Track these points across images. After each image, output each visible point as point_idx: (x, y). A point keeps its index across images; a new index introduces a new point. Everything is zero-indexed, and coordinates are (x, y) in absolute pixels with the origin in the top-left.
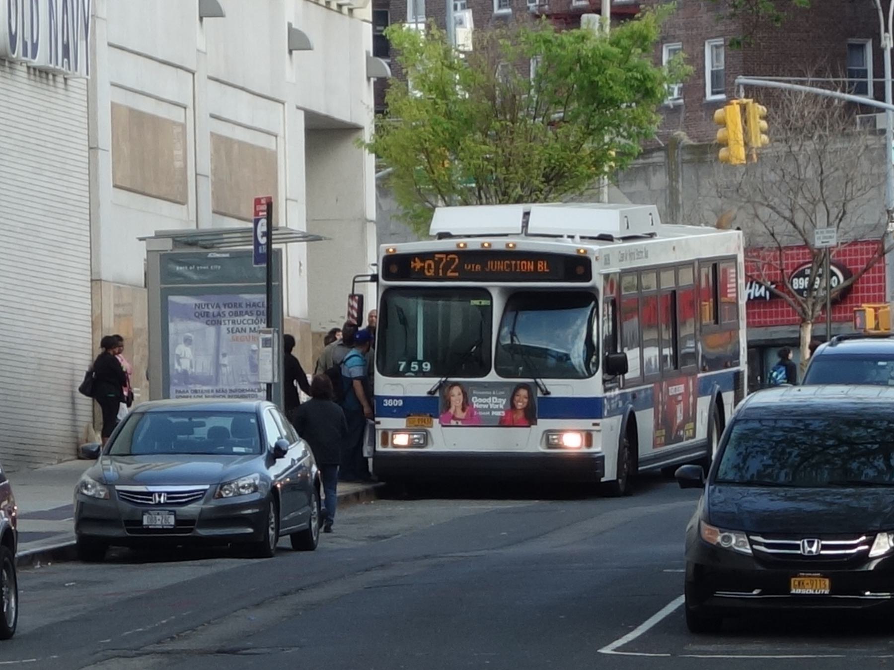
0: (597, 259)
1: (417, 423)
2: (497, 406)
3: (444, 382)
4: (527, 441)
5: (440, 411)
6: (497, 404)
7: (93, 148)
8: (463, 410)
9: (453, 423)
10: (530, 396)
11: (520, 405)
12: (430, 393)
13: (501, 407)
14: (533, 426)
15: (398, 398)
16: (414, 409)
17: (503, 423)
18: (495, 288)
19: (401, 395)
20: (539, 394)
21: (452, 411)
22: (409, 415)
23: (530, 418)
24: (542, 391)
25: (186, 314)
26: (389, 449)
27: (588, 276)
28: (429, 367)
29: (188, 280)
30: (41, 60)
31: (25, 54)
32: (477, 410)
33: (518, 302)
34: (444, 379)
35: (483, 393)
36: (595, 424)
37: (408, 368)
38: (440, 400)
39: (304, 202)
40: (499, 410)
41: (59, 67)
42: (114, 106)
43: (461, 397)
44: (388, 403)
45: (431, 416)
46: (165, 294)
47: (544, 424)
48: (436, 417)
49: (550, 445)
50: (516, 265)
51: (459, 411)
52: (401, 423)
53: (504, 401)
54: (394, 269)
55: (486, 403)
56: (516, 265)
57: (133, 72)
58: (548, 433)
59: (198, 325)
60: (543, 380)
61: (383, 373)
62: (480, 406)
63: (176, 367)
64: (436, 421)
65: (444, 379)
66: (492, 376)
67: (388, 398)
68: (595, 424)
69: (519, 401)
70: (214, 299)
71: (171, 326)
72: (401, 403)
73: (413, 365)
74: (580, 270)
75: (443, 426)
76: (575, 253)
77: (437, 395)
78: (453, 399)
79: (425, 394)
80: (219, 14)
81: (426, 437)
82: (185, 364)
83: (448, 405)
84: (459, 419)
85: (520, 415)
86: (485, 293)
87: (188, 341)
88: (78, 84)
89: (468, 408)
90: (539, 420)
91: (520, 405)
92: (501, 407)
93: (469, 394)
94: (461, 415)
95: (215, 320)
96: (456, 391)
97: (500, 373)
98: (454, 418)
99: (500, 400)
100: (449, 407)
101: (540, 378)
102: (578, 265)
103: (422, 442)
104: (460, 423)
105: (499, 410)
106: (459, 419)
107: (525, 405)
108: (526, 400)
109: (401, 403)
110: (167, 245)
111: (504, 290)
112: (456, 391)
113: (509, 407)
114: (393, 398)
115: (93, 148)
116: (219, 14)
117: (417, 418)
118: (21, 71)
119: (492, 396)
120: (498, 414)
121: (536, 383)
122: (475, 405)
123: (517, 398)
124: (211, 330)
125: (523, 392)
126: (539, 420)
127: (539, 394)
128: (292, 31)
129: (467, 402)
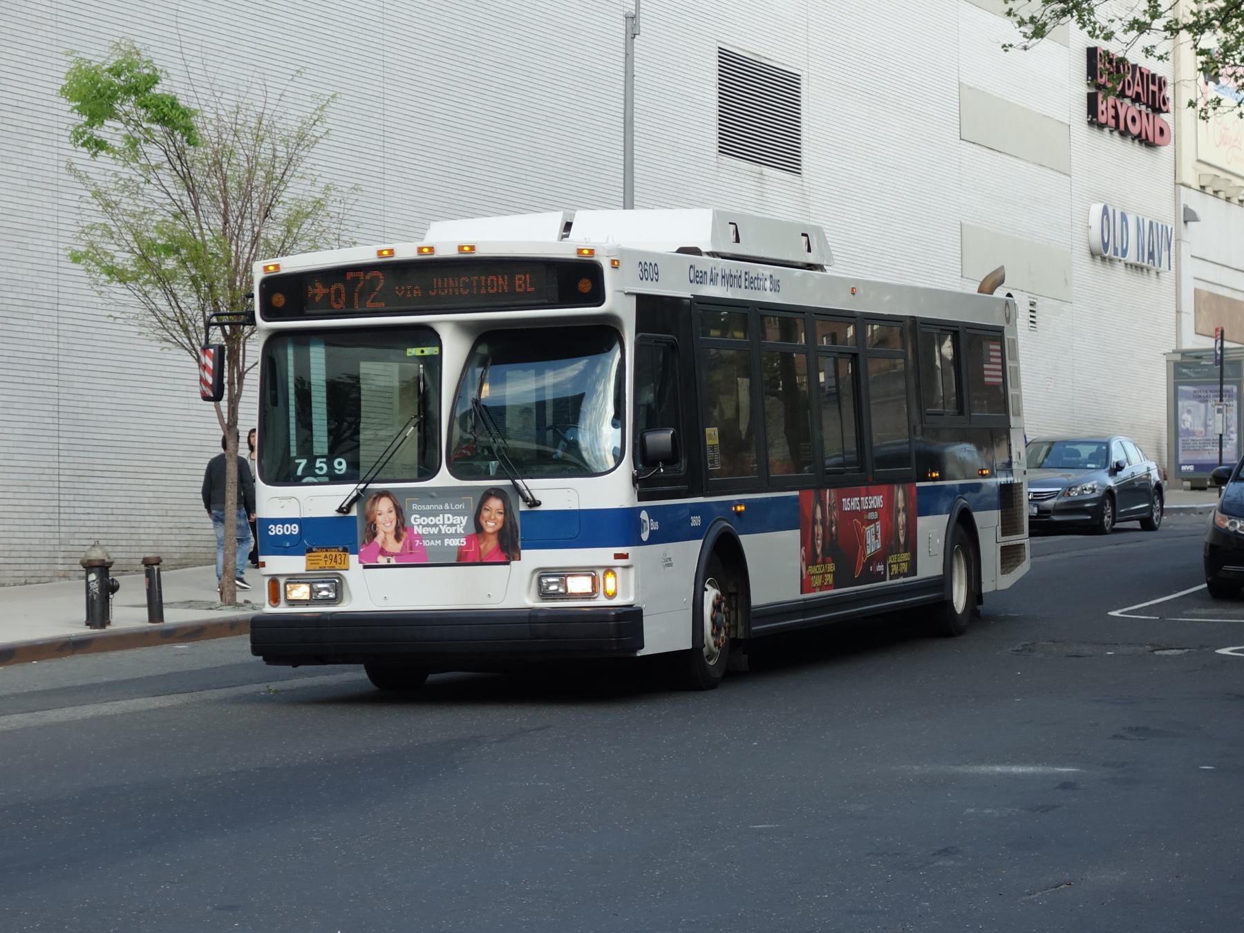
0: (615, 265)
1: (322, 564)
2: (452, 530)
3: (363, 490)
4: (507, 588)
5: (359, 541)
6: (451, 527)
7: (1178, 312)
8: (398, 538)
9: (382, 560)
10: (507, 511)
11: (491, 526)
12: (340, 510)
13: (460, 530)
14: (513, 563)
15: (291, 521)
16: (315, 536)
17: (464, 559)
18: (445, 324)
19: (297, 516)
20: (523, 507)
21: (379, 540)
22: (310, 551)
23: (508, 548)
24: (526, 500)
25: (1188, 396)
26: (283, 609)
27: (597, 296)
28: (344, 466)
29: (1190, 377)
30: (1131, 257)
31: (1116, 254)
32: (421, 537)
33: (498, 348)
34: (362, 486)
35: (429, 507)
36: (617, 556)
37: (310, 470)
38: (358, 521)
39: (965, 291)
40: (455, 535)
41: (1145, 264)
42: (1196, 291)
43: (393, 515)
44: (276, 530)
45: (345, 550)
46: (1176, 385)
47: (533, 559)
48: (355, 552)
49: (544, 595)
50: (479, 282)
51: (391, 538)
52: (296, 564)
53: (464, 520)
54: (279, 300)
55: (436, 525)
56: (479, 282)
57: (1211, 273)
58: (543, 573)
59: (1195, 403)
60: (527, 481)
61: (268, 481)
62: (425, 531)
63: (1182, 426)
64: (353, 559)
65: (362, 486)
66: (444, 478)
67: (276, 521)
68: (617, 556)
69: (490, 519)
70: (1204, 388)
71: (1180, 403)
72: (295, 529)
73: (318, 465)
74: (585, 286)
75: (365, 567)
76: (575, 257)
77: (354, 512)
78: (379, 518)
79: (332, 513)
80: (1196, 219)
81: (339, 588)
82: (1188, 425)
83: (372, 531)
84: (392, 555)
85: (490, 544)
86: (428, 335)
87: (1189, 412)
88: (1168, 277)
89: (405, 534)
90: (524, 553)
91: (491, 526)
92: (460, 530)
93: (406, 510)
94: (394, 546)
95: (1204, 400)
96: (385, 505)
97: (455, 472)
98: (383, 552)
99: (458, 519)
100: (375, 535)
101: (522, 478)
102: (579, 278)
103: (332, 595)
104: (393, 562)
105: (455, 535)
106: (392, 555)
107: (499, 525)
108: (500, 517)
109: (295, 529)
110: (1178, 357)
111: (464, 327)
112: (385, 505)
113: (472, 530)
114: (283, 521)
115: (1178, 312)
116: (1196, 219)
117: (323, 554)
118: (1121, 266)
119: (444, 512)
120: (455, 542)
121: (516, 486)
122: (417, 530)
123: (486, 514)
124: (1202, 406)
125: (495, 504)
126: (524, 553)
127: (523, 507)
128: (1186, 209)
129: (403, 524)
